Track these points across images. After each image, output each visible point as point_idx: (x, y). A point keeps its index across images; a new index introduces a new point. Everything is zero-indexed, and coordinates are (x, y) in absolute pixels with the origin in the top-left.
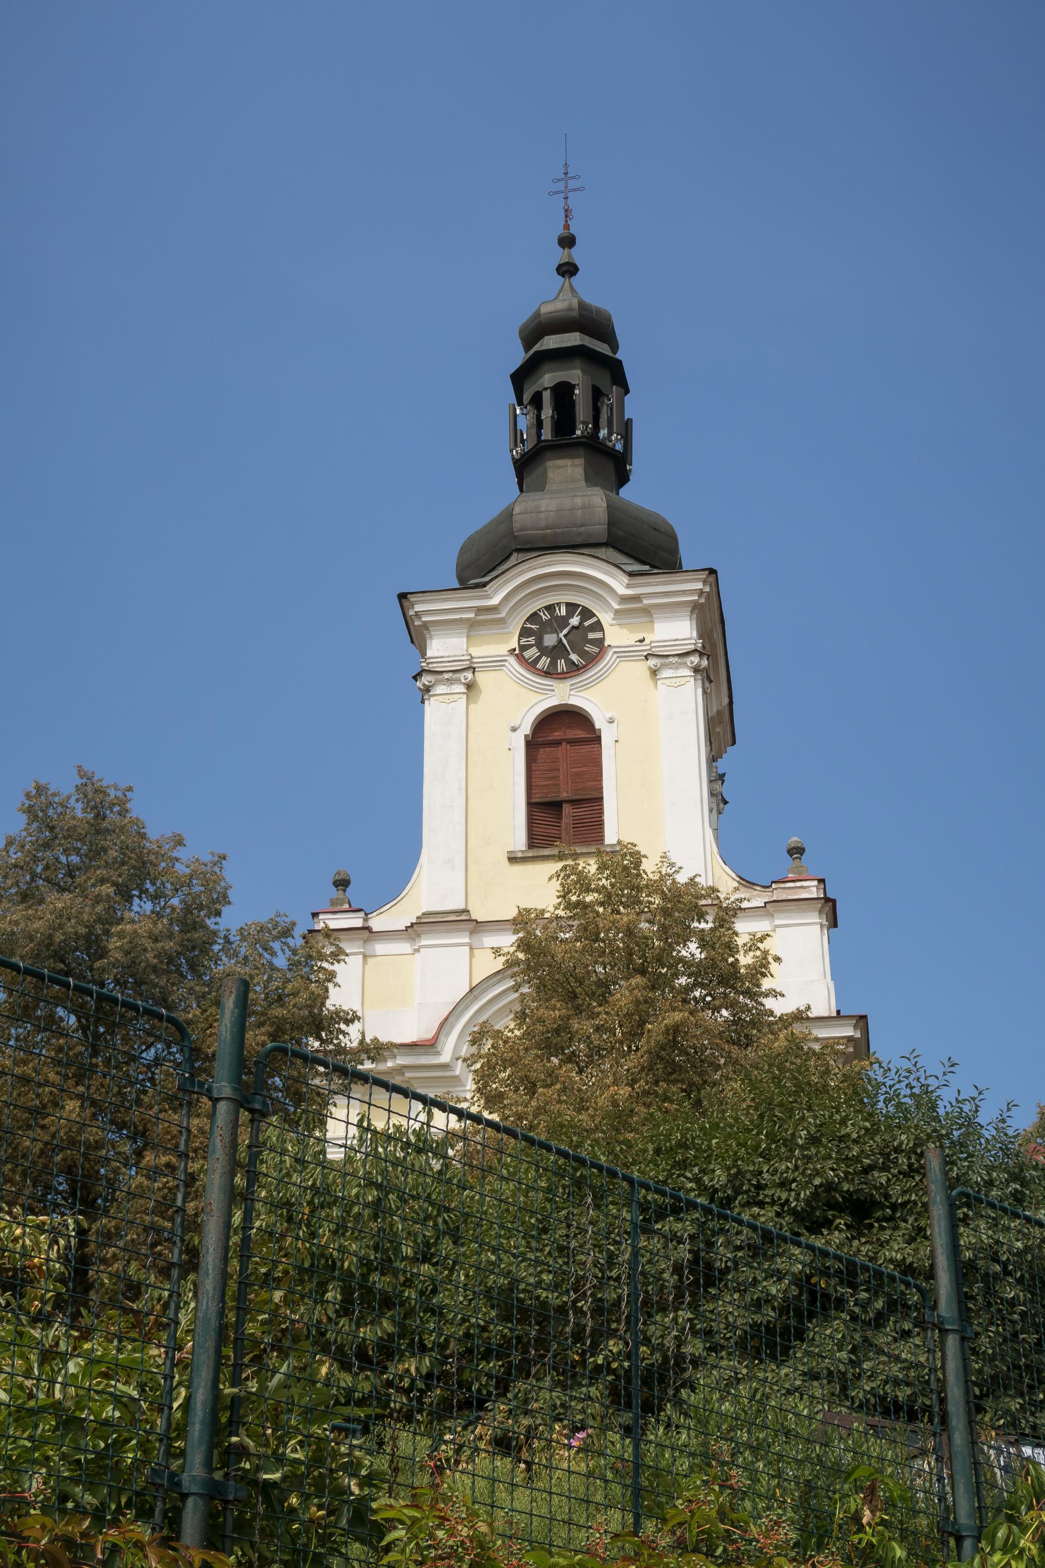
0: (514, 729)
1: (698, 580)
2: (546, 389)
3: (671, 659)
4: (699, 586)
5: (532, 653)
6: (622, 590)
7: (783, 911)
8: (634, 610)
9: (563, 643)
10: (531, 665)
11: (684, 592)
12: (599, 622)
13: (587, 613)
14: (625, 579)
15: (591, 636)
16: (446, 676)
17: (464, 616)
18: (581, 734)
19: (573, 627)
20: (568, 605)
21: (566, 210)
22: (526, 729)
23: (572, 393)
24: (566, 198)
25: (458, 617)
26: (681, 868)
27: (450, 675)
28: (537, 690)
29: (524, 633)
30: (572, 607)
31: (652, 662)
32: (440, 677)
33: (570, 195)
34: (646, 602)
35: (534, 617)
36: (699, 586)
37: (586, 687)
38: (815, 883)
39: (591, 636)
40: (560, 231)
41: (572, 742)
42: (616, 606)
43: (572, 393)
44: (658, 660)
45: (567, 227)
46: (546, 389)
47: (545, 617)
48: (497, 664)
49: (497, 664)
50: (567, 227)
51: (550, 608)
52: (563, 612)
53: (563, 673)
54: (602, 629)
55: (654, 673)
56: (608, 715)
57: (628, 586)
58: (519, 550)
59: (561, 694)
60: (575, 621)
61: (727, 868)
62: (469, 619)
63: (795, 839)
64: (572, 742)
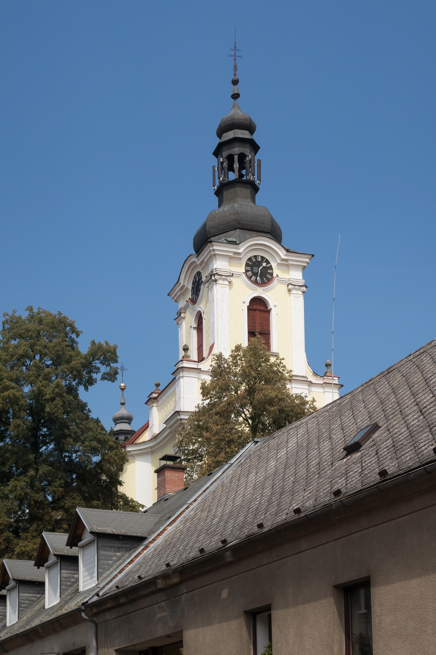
0: (244, 303)
1: (307, 258)
2: (236, 154)
3: (296, 287)
4: (308, 260)
5: (250, 273)
6: (283, 257)
7: (328, 387)
8: (285, 265)
9: (259, 272)
10: (250, 278)
11: (302, 262)
12: (271, 266)
13: (268, 262)
14: (285, 252)
15: (269, 271)
16: (223, 277)
17: (230, 254)
18: (263, 308)
19: (264, 267)
20: (262, 257)
21: (235, 66)
22: (248, 304)
23: (237, 154)
24: (235, 60)
25: (227, 254)
26: (175, 319)
27: (225, 277)
28: (251, 289)
29: (247, 265)
30: (263, 258)
31: (290, 287)
32: (221, 277)
33: (237, 58)
34: (290, 262)
35: (250, 259)
36: (308, 260)
37: (267, 291)
38: (337, 378)
39: (269, 271)
40: (232, 77)
41: (260, 311)
42: (279, 262)
43: (237, 154)
44: (291, 286)
45: (235, 75)
46: (236, 154)
47: (254, 260)
48: (239, 275)
49: (239, 275)
50: (235, 75)
51: (255, 257)
52: (260, 260)
53: (260, 284)
54: (272, 269)
55: (289, 290)
56: (275, 304)
57: (285, 255)
58: (240, 228)
59: (259, 292)
60: (264, 264)
61: (309, 368)
62: (230, 256)
63: (329, 361)
64: (260, 311)
